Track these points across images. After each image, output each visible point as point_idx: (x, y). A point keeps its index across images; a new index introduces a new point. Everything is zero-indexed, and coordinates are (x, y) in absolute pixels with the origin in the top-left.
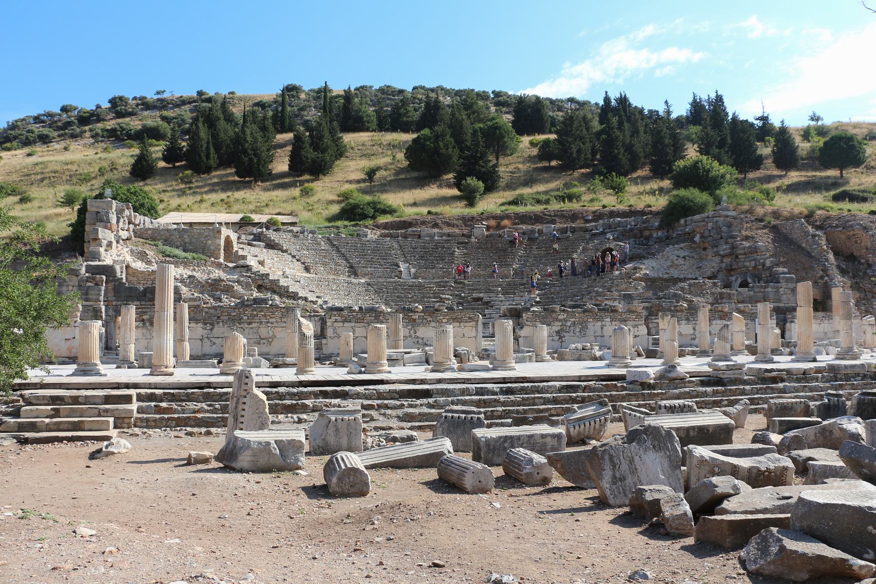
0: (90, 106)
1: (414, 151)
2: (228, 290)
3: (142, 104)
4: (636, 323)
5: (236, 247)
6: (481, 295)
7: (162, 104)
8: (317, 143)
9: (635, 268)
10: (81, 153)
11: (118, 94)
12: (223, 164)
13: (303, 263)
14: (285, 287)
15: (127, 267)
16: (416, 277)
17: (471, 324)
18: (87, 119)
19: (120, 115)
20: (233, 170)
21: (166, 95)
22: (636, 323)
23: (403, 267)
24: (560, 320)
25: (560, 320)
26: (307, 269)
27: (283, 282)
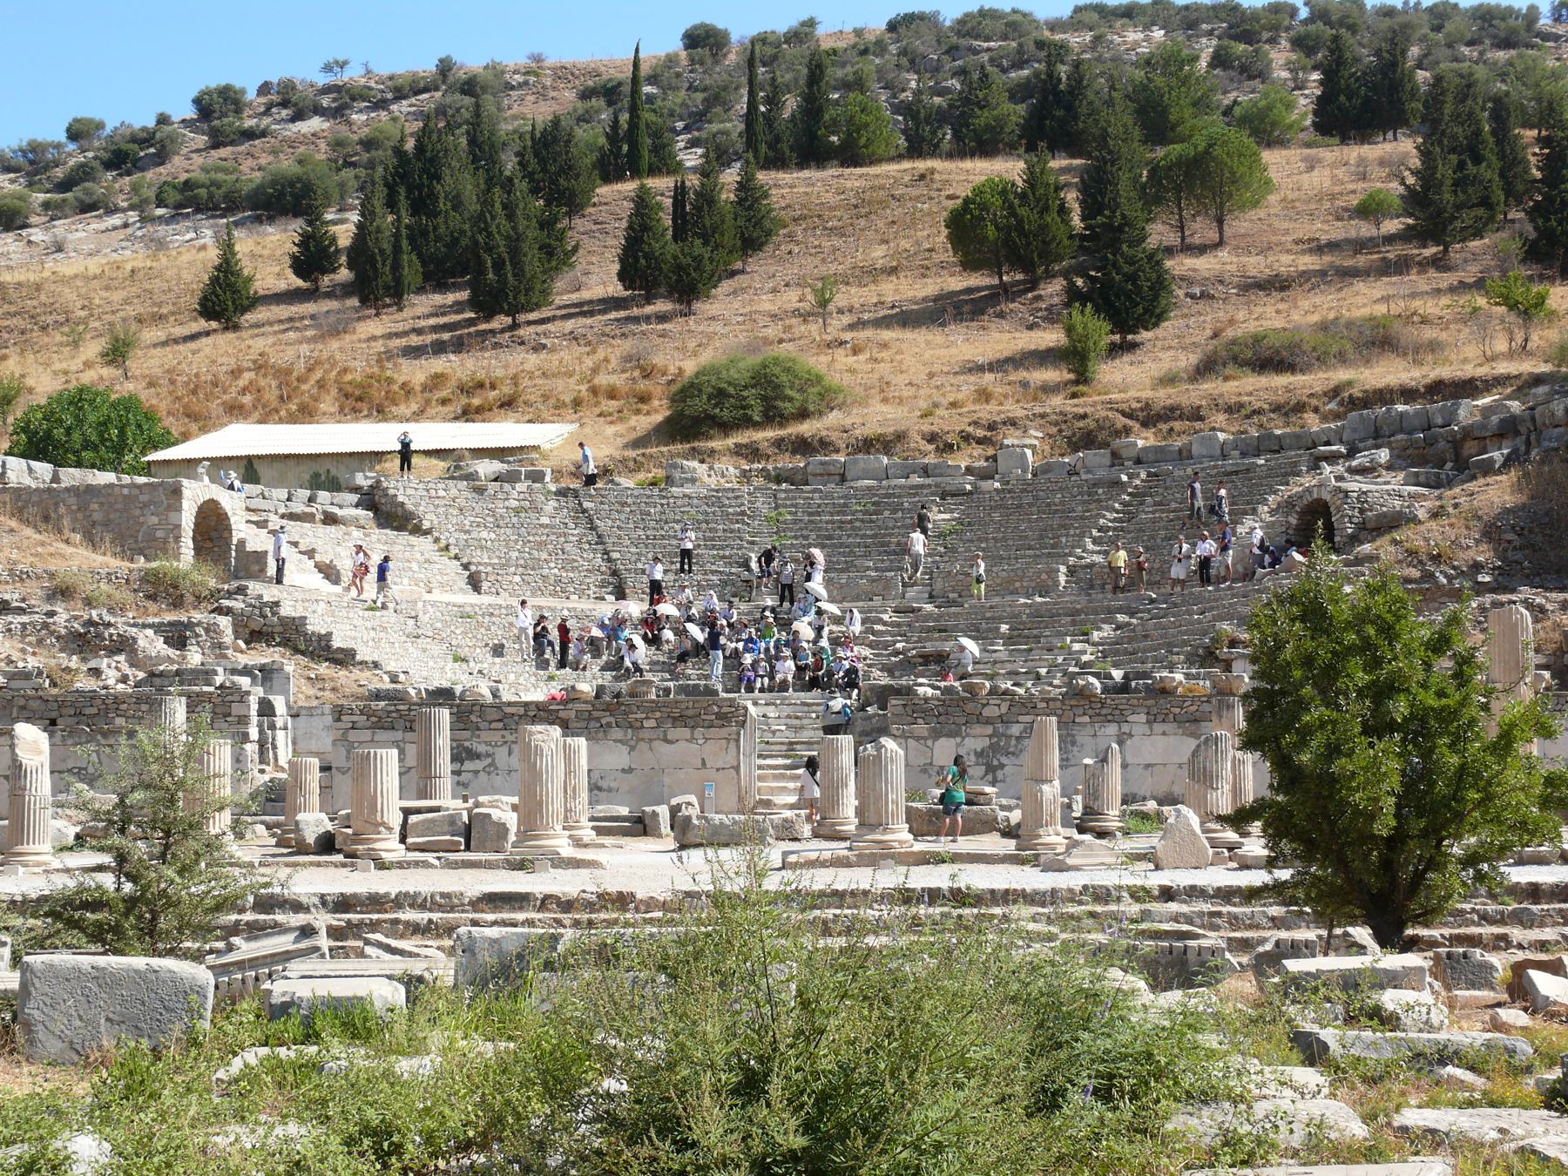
0: (144, 119)
2: (124, 645)
3: (284, 104)
5: (242, 530)
7: (341, 100)
11: (215, 81)
12: (436, 279)
13: (466, 567)
14: (320, 637)
17: (724, 732)
18: (130, 153)
20: (464, 295)
21: (353, 75)
24: (988, 721)
25: (988, 721)
26: (475, 583)
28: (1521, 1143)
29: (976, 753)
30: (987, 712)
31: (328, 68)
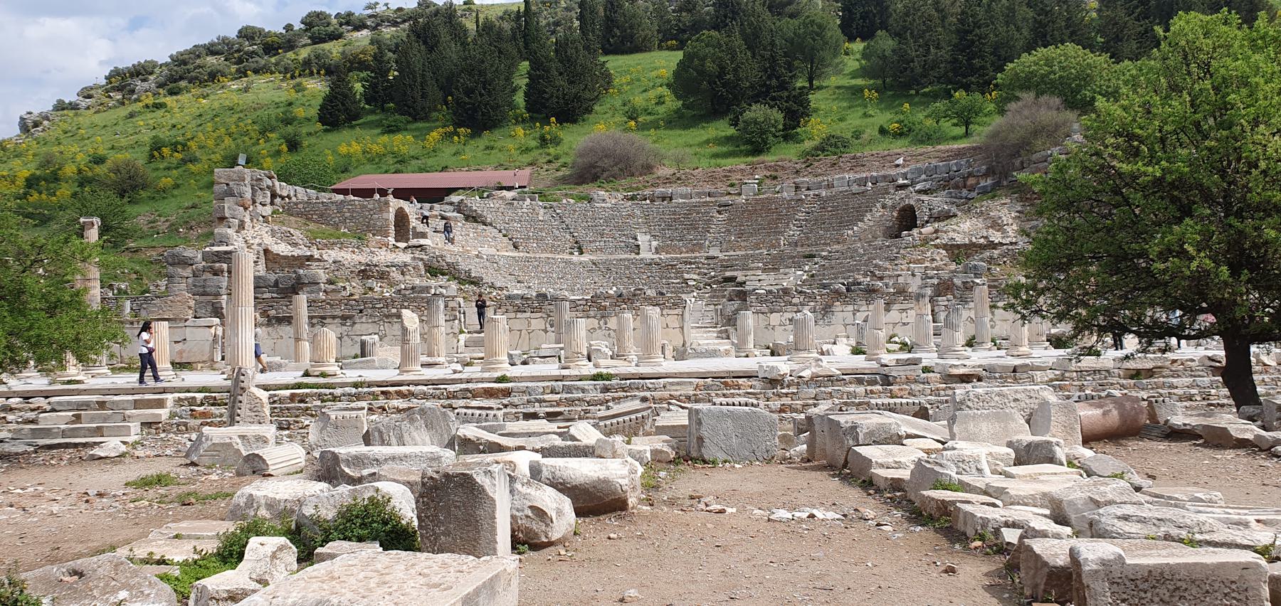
1: (683, 82)
4: (903, 306)
5: (414, 222)
6: (735, 273)
7: (379, 21)
8: (575, 72)
9: (936, 231)
10: (267, 90)
15: (266, 251)
16: (657, 251)
17: (676, 312)
18: (272, 45)
19: (317, 40)
21: (380, 9)
22: (903, 306)
23: (643, 239)
26: (516, 247)
27: (463, 266)
28: (185, 489)
29: (151, 351)
30: (794, 301)
31: (369, 7)
